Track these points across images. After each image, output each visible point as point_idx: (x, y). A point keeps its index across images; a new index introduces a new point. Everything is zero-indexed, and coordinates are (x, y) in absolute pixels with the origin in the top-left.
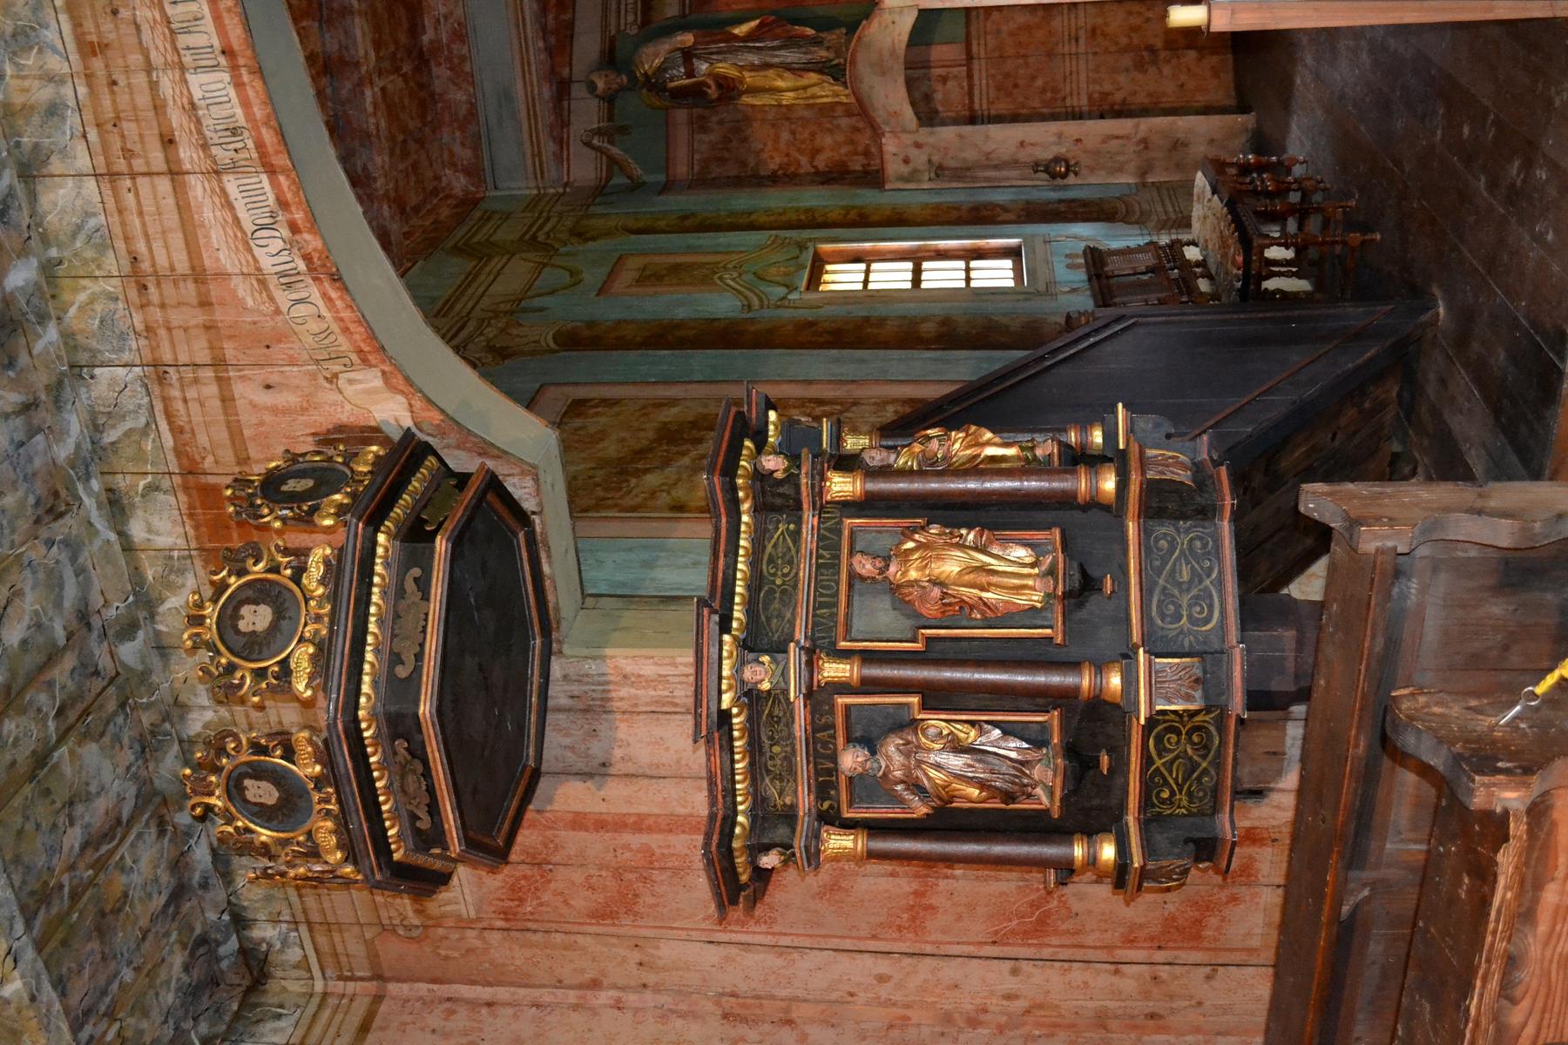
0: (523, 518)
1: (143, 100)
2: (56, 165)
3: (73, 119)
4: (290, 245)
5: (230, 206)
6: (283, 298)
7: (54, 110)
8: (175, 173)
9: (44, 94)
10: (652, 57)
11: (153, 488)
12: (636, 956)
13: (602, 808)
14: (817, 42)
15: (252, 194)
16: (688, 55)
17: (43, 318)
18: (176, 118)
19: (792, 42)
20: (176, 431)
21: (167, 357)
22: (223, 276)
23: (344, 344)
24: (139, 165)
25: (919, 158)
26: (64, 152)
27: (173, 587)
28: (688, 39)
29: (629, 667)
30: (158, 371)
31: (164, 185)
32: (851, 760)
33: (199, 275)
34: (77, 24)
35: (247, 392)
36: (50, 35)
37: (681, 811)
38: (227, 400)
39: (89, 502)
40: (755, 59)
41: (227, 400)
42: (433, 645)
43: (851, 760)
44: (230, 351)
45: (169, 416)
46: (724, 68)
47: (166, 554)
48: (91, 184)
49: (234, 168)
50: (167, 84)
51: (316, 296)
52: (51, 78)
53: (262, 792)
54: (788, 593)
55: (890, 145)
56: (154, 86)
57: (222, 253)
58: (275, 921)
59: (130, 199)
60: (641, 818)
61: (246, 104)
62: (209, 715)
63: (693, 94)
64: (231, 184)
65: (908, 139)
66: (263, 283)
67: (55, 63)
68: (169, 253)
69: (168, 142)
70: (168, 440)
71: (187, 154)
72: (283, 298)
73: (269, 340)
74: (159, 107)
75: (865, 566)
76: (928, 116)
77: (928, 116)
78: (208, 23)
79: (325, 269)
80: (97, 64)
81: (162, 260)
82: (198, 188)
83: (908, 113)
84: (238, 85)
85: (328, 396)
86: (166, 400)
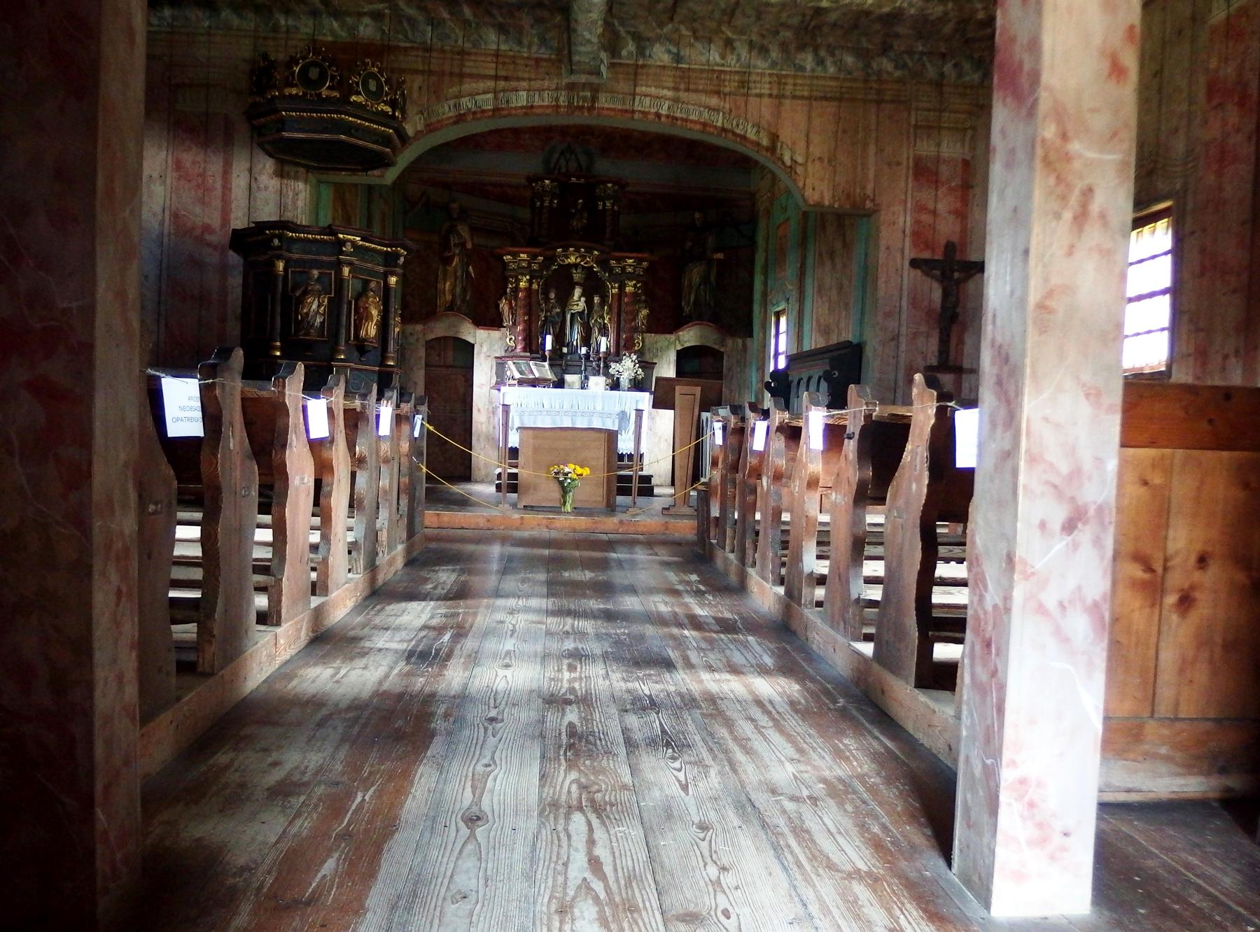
0: (366, 170)
1: (520, 74)
2: (503, 38)
3: (517, 48)
4: (469, 110)
5: (484, 93)
6: (452, 103)
7: (520, 43)
8: (496, 78)
9: (526, 42)
10: (464, 230)
11: (383, 31)
12: (155, 175)
13: (234, 175)
14: (464, 301)
15: (487, 102)
16: (463, 245)
17: (451, 14)
18: (514, 84)
19: (464, 290)
20: (406, 49)
21: (434, 54)
22: (461, 83)
23: (434, 119)
24: (500, 66)
25: (412, 340)
26: (506, 41)
27: (343, 25)
28: (469, 246)
29: (302, 196)
30: (429, 49)
31: (492, 73)
32: (315, 273)
33: (462, 76)
34: (545, 60)
35: (418, 81)
36: (543, 50)
37: (233, 206)
38: (416, 72)
39: (380, 6)
40: (459, 273)
41: (416, 72)
42: (360, 142)
43: (315, 273)
44: (434, 78)
45: (412, 48)
46: (456, 260)
47: (355, 28)
48: (494, 47)
49: (496, 98)
50: (524, 84)
51: (451, 114)
52: (530, 47)
53: (314, 73)
54: (362, 260)
55: (419, 327)
56: (523, 79)
57: (468, 86)
58: (174, 18)
59: (489, 59)
60: (230, 190)
61: (516, 108)
62: (283, 22)
63: (445, 245)
64: (490, 96)
65: (421, 336)
66: (457, 97)
67: (534, 49)
68: (469, 67)
69: (506, 79)
70: (402, 44)
71: (502, 84)
72: (452, 103)
73: (437, 93)
74: (518, 79)
75: (373, 285)
76: (430, 345)
77: (430, 345)
78: (541, 103)
79: (460, 119)
80: (532, 63)
81: (467, 64)
82: (490, 84)
83: (432, 336)
84: (522, 107)
85: (416, 109)
86: (418, 49)
